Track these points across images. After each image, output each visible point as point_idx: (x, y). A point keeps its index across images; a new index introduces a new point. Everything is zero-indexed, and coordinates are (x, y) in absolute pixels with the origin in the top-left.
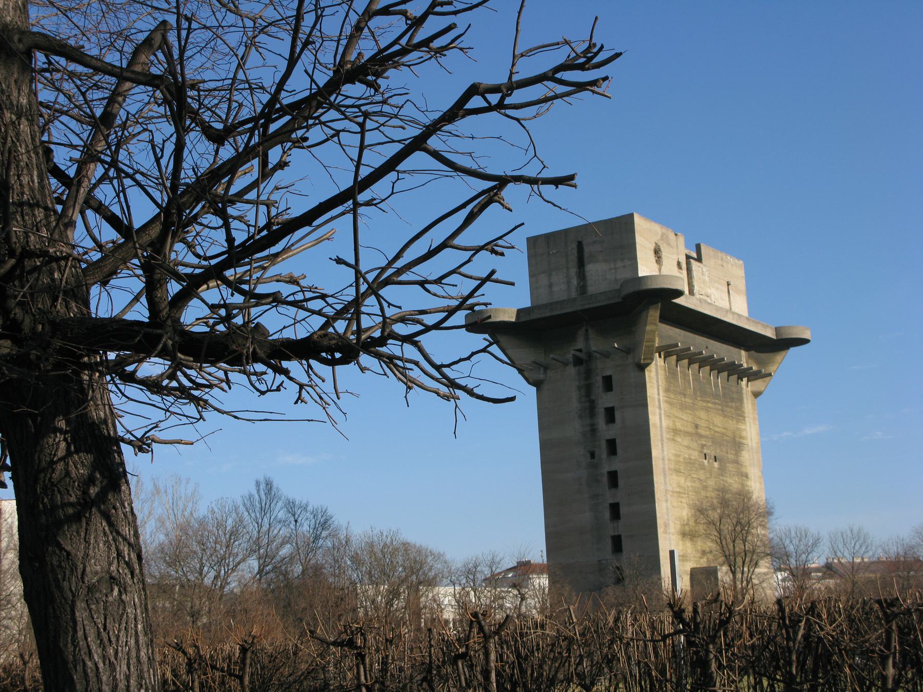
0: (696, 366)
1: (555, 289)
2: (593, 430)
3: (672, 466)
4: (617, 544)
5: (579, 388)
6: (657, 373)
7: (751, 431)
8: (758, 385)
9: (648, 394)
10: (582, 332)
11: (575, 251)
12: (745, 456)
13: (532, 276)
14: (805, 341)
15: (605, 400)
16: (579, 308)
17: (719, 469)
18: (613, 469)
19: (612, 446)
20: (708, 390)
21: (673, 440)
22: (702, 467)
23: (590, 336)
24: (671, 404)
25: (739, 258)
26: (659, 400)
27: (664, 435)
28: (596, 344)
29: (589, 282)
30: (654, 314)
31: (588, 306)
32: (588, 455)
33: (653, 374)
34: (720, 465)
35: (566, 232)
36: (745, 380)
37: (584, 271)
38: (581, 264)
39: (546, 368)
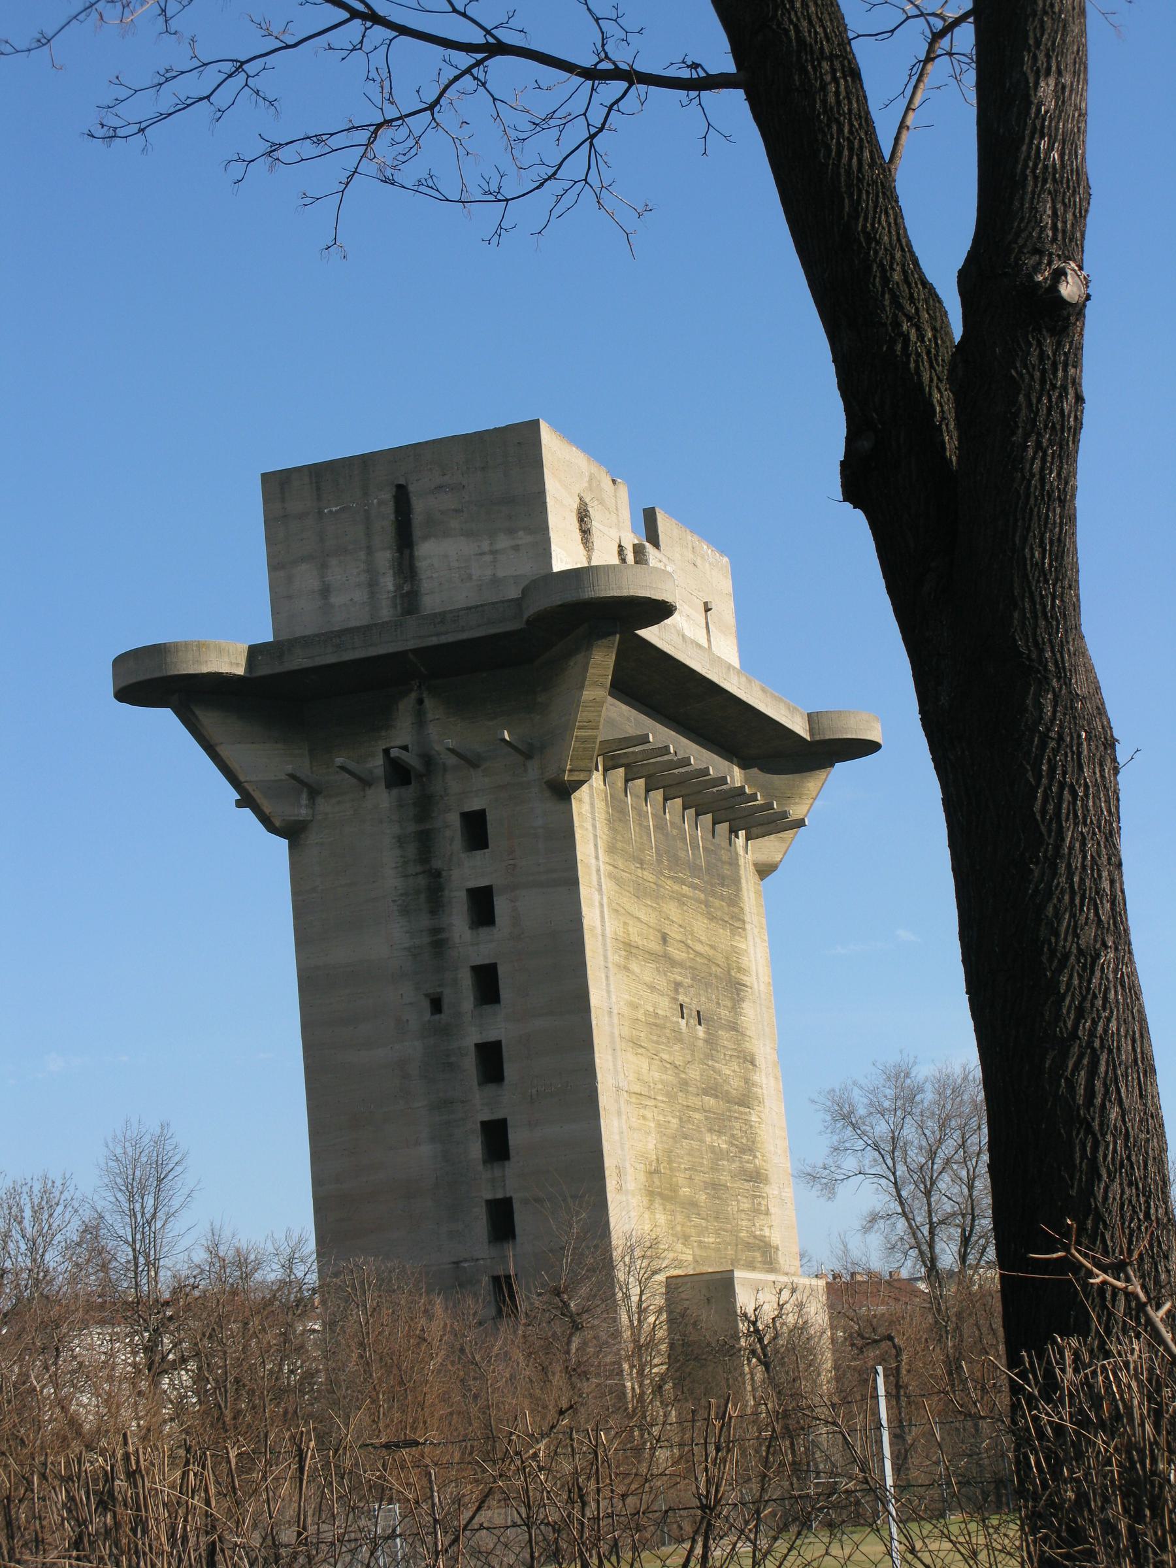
0: (658, 795)
1: (336, 600)
2: (439, 943)
3: (626, 1032)
4: (502, 1220)
5: (401, 841)
6: (592, 805)
7: (756, 954)
8: (768, 848)
9: (579, 856)
10: (406, 705)
11: (389, 510)
12: (748, 1008)
13: (275, 565)
14: (868, 747)
15: (468, 871)
16: (412, 644)
17: (706, 1041)
18: (491, 1036)
19: (487, 983)
20: (682, 854)
21: (626, 969)
22: (678, 1037)
23: (430, 716)
24: (618, 881)
25: (723, 552)
26: (598, 871)
27: (610, 954)
28: (447, 735)
29: (426, 586)
30: (602, 662)
31: (434, 641)
32: (426, 1004)
33: (586, 808)
34: (707, 1033)
35: (365, 461)
36: (742, 834)
37: (412, 557)
38: (404, 538)
39: (314, 792)
